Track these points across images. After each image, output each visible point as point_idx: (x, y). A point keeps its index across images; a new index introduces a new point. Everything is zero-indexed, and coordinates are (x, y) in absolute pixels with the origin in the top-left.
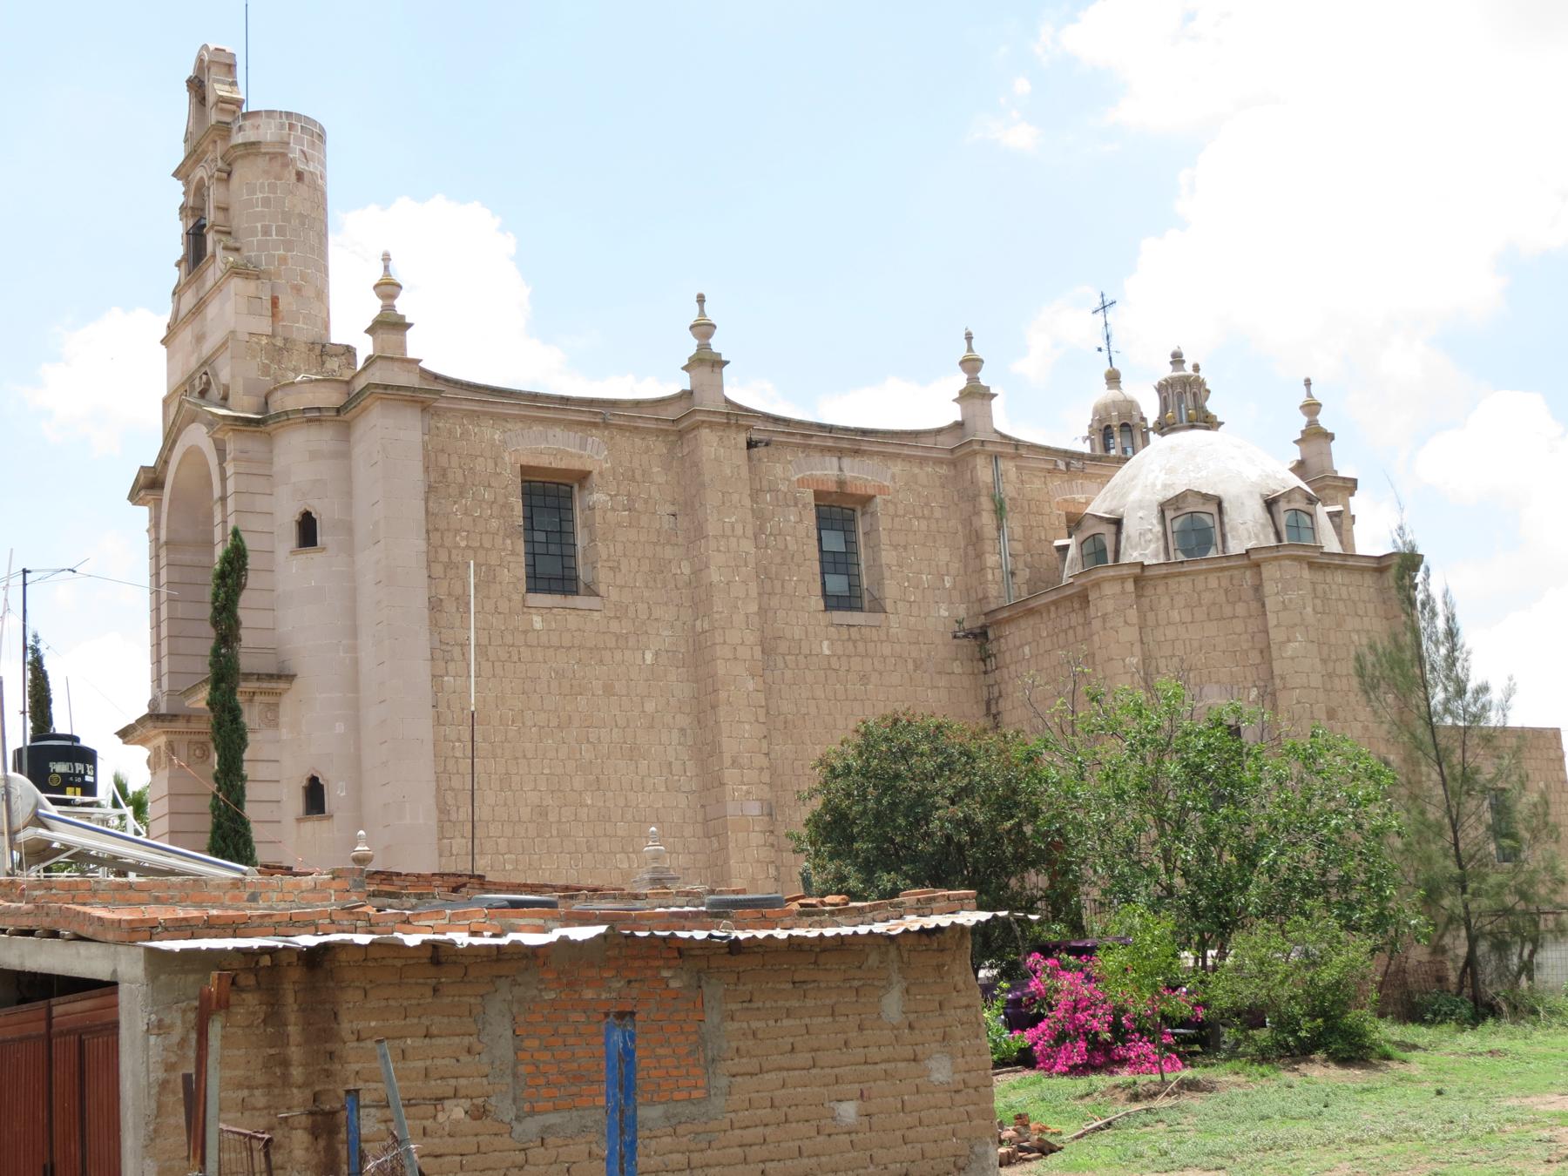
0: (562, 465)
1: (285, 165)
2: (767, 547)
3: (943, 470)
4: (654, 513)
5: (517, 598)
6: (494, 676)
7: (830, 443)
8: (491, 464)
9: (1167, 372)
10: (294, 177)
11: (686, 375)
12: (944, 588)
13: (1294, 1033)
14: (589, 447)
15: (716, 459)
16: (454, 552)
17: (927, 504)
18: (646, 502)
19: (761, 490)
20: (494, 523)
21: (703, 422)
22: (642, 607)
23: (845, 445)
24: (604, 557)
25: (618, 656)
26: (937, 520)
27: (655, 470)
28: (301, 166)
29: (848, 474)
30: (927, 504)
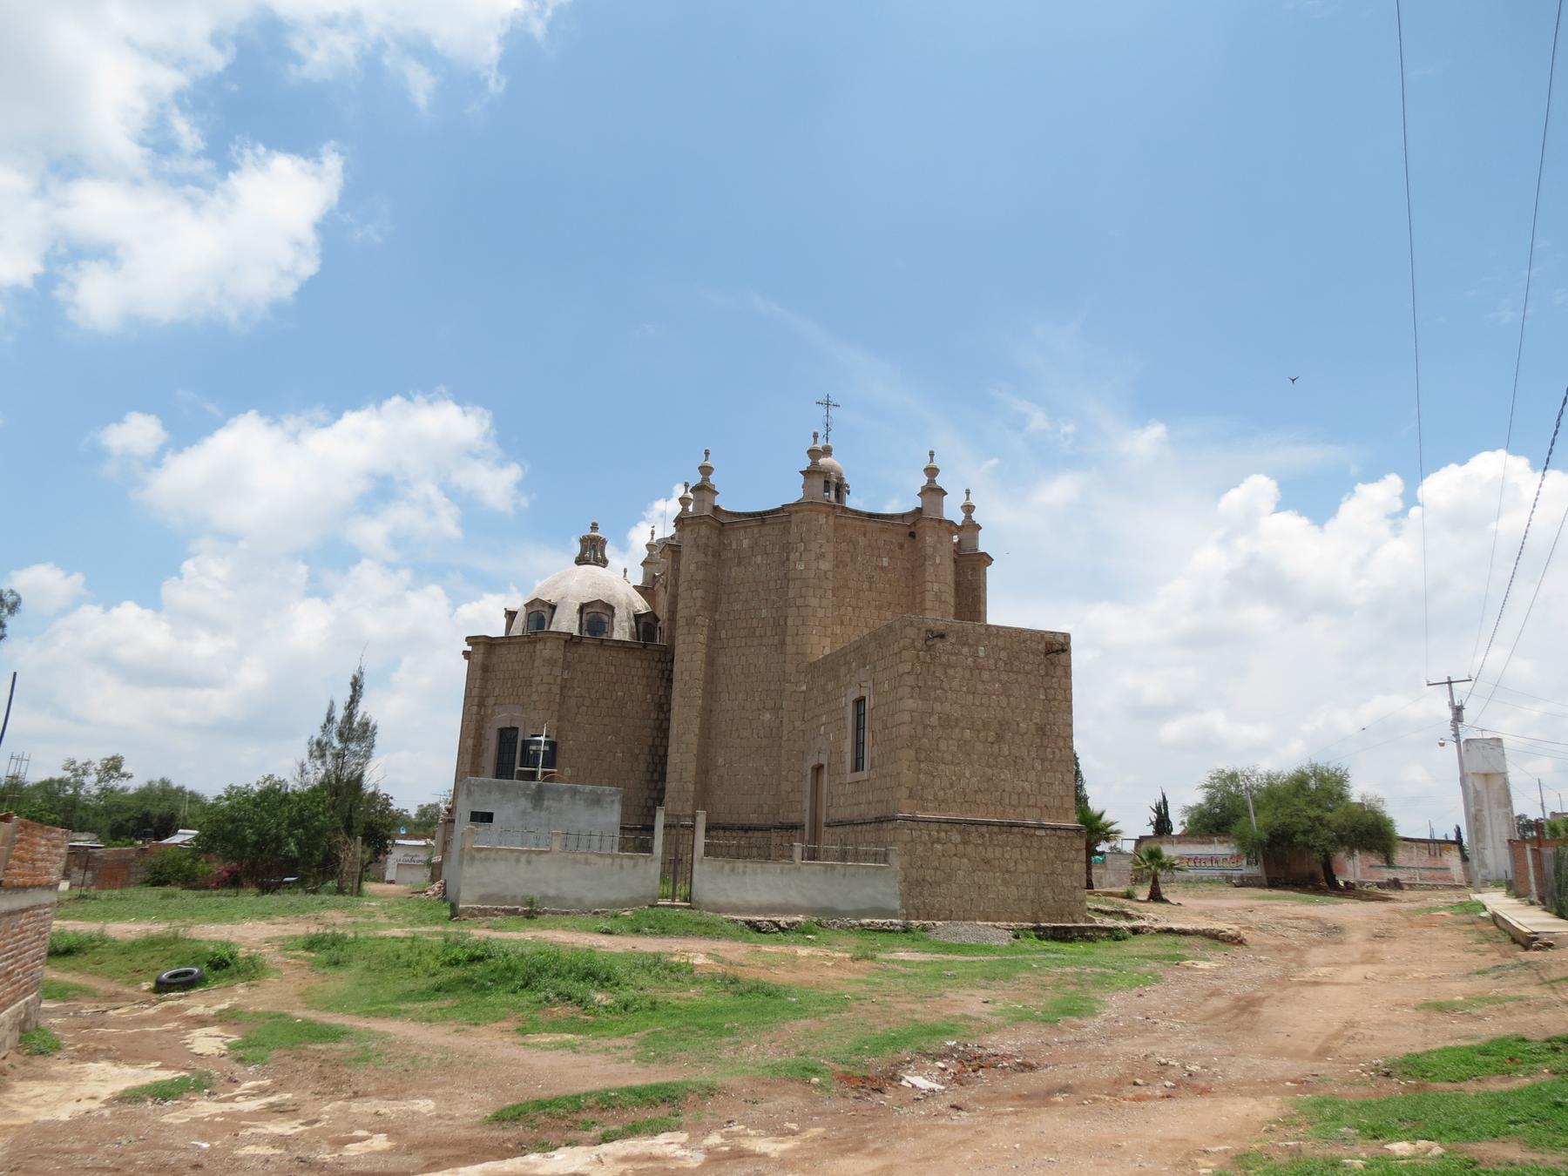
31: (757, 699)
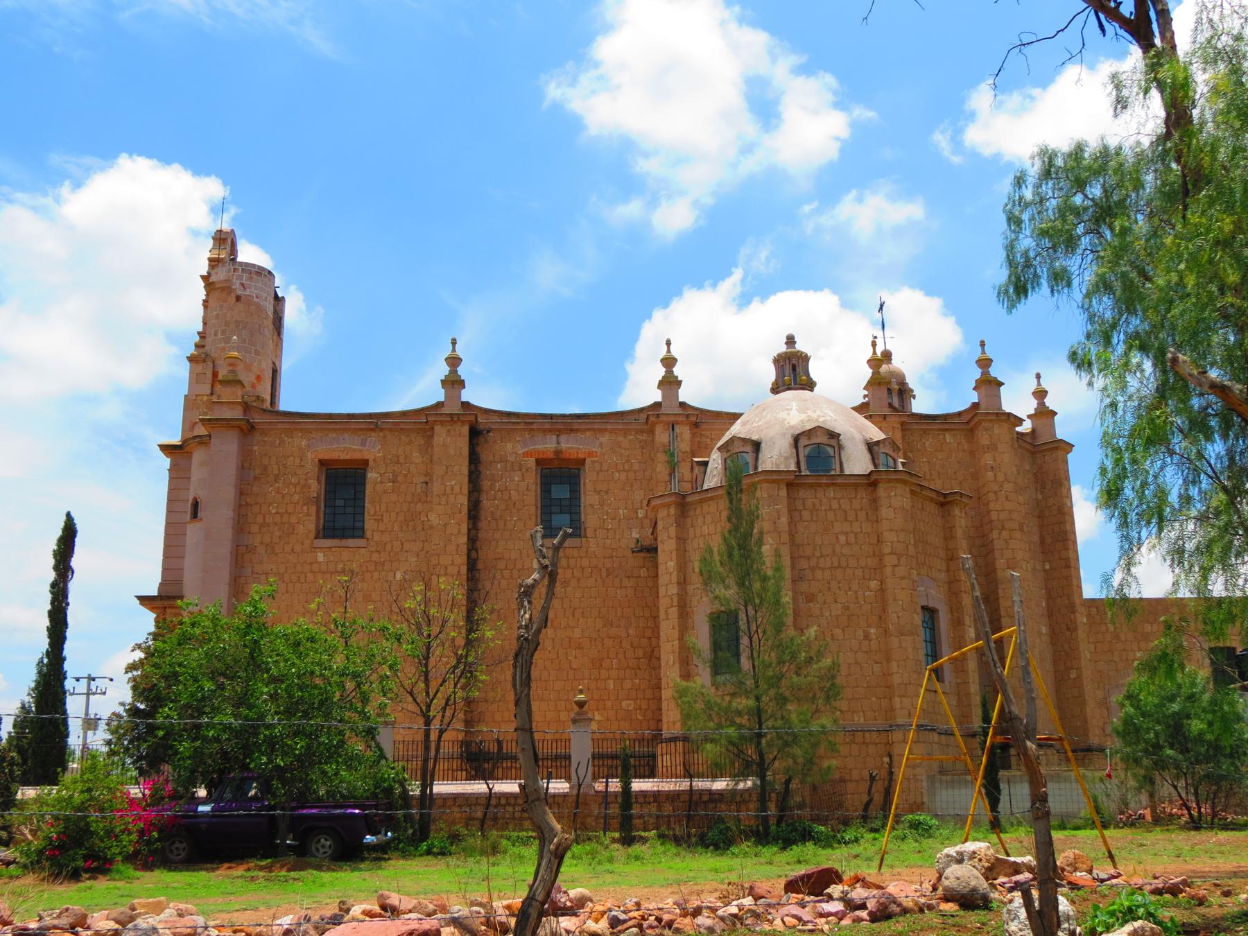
0: (348, 457)
1: (230, 293)
2: (495, 499)
3: (643, 437)
4: (411, 483)
5: (307, 542)
6: (287, 592)
7: (547, 426)
8: (298, 461)
9: (783, 348)
10: (234, 300)
11: (975, 393)
12: (637, 518)
13: (1221, 810)
14: (367, 444)
15: (444, 445)
16: (267, 516)
17: (627, 462)
18: (406, 476)
19: (494, 462)
20: (296, 497)
21: (435, 421)
22: (397, 544)
23: (560, 427)
24: (372, 513)
25: (376, 575)
26: (635, 472)
27: (415, 454)
28: (239, 293)
29: (564, 446)
30: (627, 462)
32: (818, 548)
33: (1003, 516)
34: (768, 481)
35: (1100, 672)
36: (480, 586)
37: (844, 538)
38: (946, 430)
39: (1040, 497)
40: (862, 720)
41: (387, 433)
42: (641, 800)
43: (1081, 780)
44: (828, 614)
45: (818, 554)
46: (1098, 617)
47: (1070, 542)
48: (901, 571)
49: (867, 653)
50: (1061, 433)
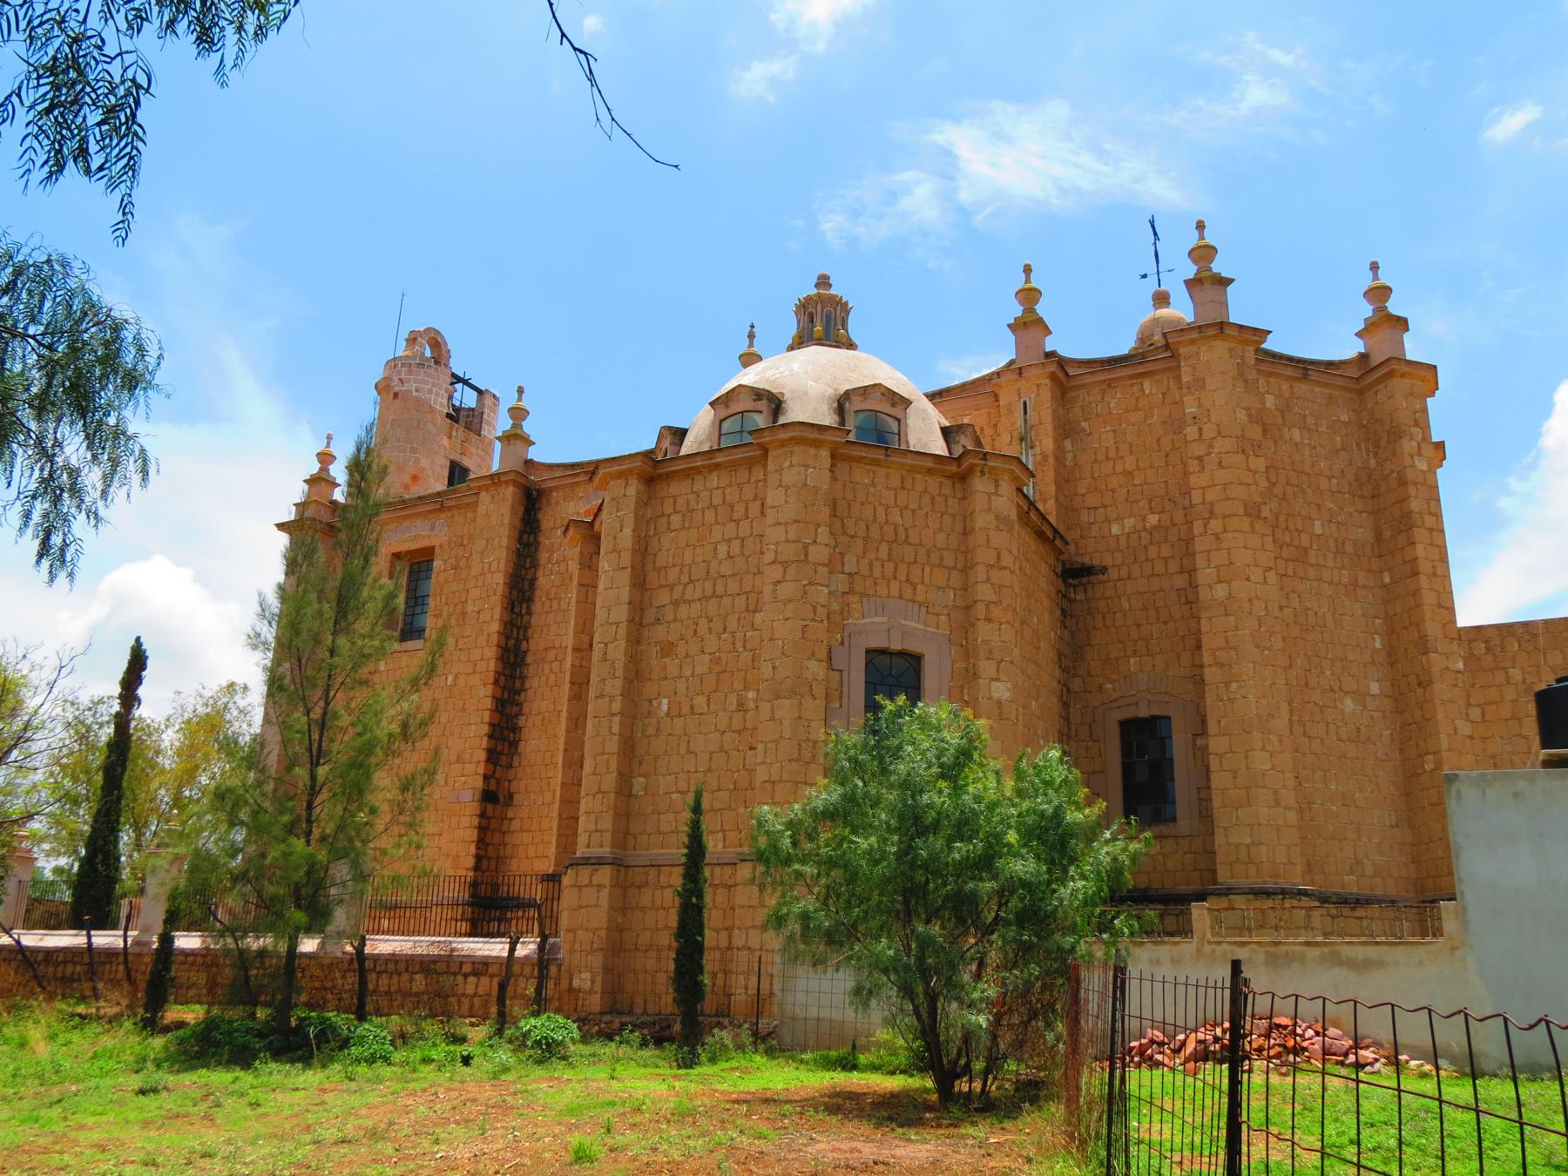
31: (1328, 673)
32: (686, 569)
33: (1212, 495)
34: (620, 475)
35: (1493, 757)
36: (527, 686)
37: (725, 548)
38: (1143, 375)
39: (1373, 463)
40: (720, 845)
41: (455, 511)
42: (391, 967)
43: (670, 947)
44: (688, 673)
45: (685, 579)
46: (1489, 658)
47: (1420, 534)
48: (786, 590)
49: (739, 732)
50: (1414, 348)
